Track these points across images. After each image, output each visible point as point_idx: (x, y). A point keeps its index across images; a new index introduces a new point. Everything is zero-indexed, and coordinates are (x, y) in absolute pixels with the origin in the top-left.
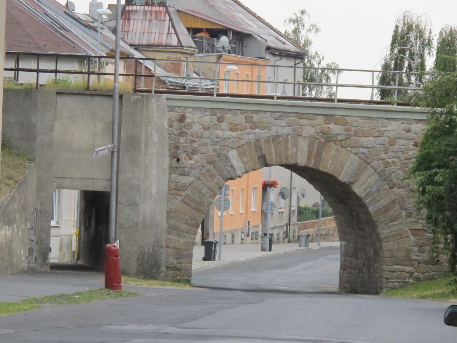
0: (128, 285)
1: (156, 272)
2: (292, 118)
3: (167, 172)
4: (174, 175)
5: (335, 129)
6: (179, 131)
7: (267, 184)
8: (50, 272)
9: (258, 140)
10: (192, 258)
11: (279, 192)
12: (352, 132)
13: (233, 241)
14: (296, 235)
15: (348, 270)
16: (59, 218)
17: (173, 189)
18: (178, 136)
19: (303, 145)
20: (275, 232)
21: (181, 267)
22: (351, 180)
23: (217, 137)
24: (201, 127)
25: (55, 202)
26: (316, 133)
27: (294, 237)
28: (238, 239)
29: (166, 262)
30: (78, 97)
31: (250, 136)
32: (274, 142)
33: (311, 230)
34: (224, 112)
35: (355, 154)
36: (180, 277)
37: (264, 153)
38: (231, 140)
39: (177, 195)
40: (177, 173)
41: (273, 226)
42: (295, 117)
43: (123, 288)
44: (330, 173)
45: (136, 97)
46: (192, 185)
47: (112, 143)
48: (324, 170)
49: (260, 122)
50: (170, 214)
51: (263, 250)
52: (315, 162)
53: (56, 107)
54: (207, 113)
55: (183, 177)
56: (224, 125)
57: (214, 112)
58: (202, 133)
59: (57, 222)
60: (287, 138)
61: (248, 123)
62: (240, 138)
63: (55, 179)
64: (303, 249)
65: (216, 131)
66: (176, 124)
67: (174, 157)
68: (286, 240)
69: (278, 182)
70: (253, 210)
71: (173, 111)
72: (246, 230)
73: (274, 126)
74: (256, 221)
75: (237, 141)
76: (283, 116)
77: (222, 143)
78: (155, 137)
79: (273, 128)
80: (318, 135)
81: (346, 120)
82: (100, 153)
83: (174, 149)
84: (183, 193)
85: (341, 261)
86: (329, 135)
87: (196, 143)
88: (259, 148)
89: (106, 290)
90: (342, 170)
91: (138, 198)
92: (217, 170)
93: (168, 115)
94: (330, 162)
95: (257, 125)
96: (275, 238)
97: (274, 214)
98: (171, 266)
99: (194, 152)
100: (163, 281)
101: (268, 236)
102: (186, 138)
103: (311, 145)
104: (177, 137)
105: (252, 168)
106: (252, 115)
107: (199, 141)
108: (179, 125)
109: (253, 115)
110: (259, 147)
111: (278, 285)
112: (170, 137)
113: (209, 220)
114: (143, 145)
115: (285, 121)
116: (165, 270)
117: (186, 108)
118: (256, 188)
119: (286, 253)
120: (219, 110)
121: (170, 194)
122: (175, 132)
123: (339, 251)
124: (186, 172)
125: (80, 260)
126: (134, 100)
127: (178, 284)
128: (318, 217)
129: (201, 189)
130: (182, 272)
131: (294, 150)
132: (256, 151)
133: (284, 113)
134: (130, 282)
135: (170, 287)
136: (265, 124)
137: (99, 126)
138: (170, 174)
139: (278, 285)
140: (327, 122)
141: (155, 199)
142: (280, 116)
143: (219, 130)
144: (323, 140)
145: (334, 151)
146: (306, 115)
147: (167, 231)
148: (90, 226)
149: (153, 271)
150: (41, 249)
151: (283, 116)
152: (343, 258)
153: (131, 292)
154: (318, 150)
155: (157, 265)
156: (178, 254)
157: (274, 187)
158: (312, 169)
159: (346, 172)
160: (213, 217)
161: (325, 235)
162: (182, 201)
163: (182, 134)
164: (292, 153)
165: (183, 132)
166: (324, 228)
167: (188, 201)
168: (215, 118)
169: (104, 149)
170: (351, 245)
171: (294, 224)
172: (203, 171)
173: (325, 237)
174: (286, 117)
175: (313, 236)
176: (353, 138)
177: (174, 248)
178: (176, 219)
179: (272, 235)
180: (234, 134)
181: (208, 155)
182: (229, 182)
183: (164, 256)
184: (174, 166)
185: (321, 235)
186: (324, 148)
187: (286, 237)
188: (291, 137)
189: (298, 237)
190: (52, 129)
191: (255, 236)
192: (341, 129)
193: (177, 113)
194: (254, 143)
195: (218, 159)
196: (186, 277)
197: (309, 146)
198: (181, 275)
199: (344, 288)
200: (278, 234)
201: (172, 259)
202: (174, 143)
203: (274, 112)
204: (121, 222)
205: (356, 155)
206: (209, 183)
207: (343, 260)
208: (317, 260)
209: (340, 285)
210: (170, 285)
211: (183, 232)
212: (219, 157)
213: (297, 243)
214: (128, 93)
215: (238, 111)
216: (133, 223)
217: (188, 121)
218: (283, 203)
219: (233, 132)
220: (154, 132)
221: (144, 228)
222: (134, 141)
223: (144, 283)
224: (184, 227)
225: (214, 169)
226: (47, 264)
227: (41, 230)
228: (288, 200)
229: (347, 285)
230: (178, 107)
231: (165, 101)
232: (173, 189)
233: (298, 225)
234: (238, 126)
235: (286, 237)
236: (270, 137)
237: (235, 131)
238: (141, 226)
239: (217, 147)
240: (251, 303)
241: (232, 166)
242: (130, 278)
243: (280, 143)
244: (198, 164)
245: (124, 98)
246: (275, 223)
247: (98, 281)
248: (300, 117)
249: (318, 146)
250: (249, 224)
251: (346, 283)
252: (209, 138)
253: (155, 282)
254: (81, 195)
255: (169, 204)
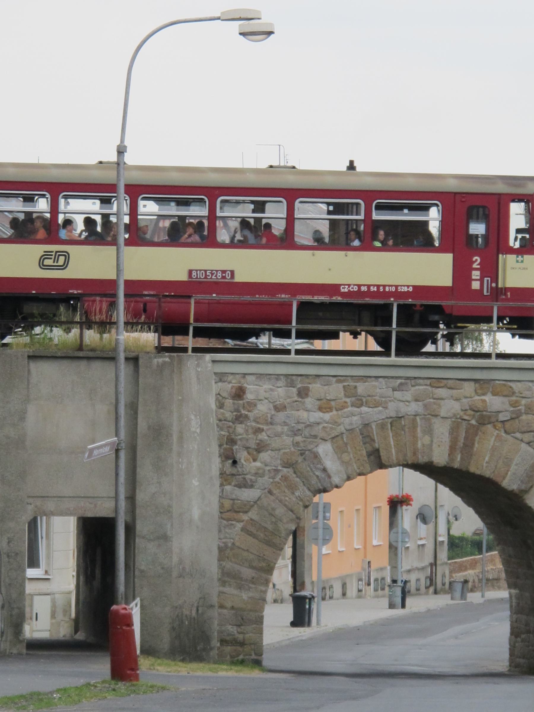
0: (154, 672)
1: (204, 649)
2: (421, 387)
3: (217, 482)
4: (228, 488)
5: (494, 402)
6: (235, 413)
7: (396, 499)
8: (27, 654)
9: (367, 425)
10: (262, 623)
11: (417, 512)
12: (522, 408)
13: (344, 594)
14: (447, 581)
15: (523, 636)
16: (48, 564)
17: (228, 511)
18: (233, 423)
19: (442, 430)
20: (412, 578)
21: (244, 639)
22: (523, 487)
23: (298, 423)
24: (271, 406)
25: (42, 538)
26: (462, 410)
27: (444, 584)
28: (352, 591)
29: (220, 632)
30: (65, 362)
31: (353, 418)
32: (393, 428)
33: (471, 572)
34: (307, 381)
35: (528, 443)
36: (244, 656)
37: (377, 446)
38: (321, 426)
39: (235, 520)
40: (233, 484)
41: (409, 568)
42: (426, 385)
43: (141, 676)
44: (487, 476)
45: (160, 360)
46: (258, 502)
47: (117, 434)
48: (478, 472)
49: (369, 396)
50: (222, 551)
51: (392, 606)
52: (462, 458)
53: (28, 380)
54: (280, 383)
55: (243, 489)
56: (309, 401)
57: (292, 380)
58: (272, 415)
59: (46, 572)
60: (414, 420)
61: (349, 397)
62: (336, 422)
63: (31, 500)
64: (458, 604)
65: (296, 412)
66: (229, 403)
67: (227, 458)
68: (431, 589)
69: (413, 497)
70: (375, 543)
71: (224, 382)
72: (365, 576)
73: (393, 401)
74: (381, 560)
75: (331, 428)
76: (406, 384)
77: (306, 432)
78: (195, 425)
79: (391, 405)
80: (465, 414)
81: (511, 387)
82: (96, 452)
83: (227, 444)
84: (245, 517)
85: (512, 622)
86: (484, 413)
87: (264, 433)
88: (367, 438)
89: (113, 682)
90: (508, 471)
91: (169, 526)
92: (300, 478)
93: (215, 388)
94: (487, 459)
95: (364, 400)
96: (412, 586)
97: (410, 549)
98: (228, 638)
99: (261, 448)
100: (215, 663)
101: (400, 583)
102: (246, 425)
103: (454, 431)
104: (231, 424)
105: (358, 471)
106: (355, 384)
107: (268, 430)
108: (234, 404)
109: (357, 384)
110: (369, 436)
111: (409, 665)
112: (220, 424)
113: (304, 561)
114: (175, 438)
115: (410, 392)
116: (219, 645)
117: (244, 375)
118: (379, 507)
119: (429, 611)
120: (299, 378)
121: (224, 519)
122: (229, 415)
123: (508, 606)
124: (249, 481)
125: (79, 633)
126: (158, 366)
127: (239, 668)
128: (480, 552)
129: (274, 509)
130: (247, 649)
131: (427, 440)
132: (364, 443)
133: (408, 378)
134: (159, 668)
135: (227, 673)
136: (377, 398)
137: (103, 410)
138: (222, 485)
139: (409, 665)
140: (480, 392)
141: (198, 527)
142: (401, 384)
143: (301, 411)
144: (473, 422)
145: (493, 438)
146: (445, 381)
147: (219, 580)
148: (93, 576)
149: (198, 648)
150: (11, 615)
151: (406, 384)
152: (515, 616)
153: (155, 684)
154: (466, 438)
155: (206, 638)
156: (240, 618)
157: (407, 505)
158: (458, 471)
159: (514, 474)
160: (119, 544)
161: (494, 579)
162: (242, 529)
163: (239, 418)
164: (423, 445)
165: (241, 415)
166: (492, 569)
167: (253, 530)
168: (294, 390)
169: (103, 444)
170: (527, 594)
171: (443, 564)
172: (277, 479)
173: (492, 583)
174: (412, 386)
175: (474, 581)
176: (524, 417)
177: (233, 608)
178: (233, 560)
179: (406, 582)
180: (327, 416)
181: (284, 453)
182: (326, 497)
183: (216, 622)
184: (228, 472)
185: (488, 580)
186: (476, 435)
187: (431, 584)
188: (421, 419)
189: (450, 583)
190: (22, 418)
191: (380, 584)
192: (503, 403)
193: (231, 385)
194: (360, 430)
195: (300, 459)
196: (254, 657)
197: (451, 433)
198: (245, 652)
199: (517, 666)
200: (418, 580)
201: (229, 627)
202: (227, 434)
203: (392, 377)
204: (143, 568)
205: (530, 446)
206: (287, 499)
207: (514, 619)
208: (478, 620)
209: (511, 661)
210: (226, 670)
211: (246, 580)
212: (302, 454)
213: (449, 593)
214: (148, 353)
215: (331, 378)
216: (163, 568)
217: (249, 396)
218: (423, 530)
219: (324, 412)
220: (193, 417)
221: (180, 576)
222: (159, 432)
223: (183, 669)
224: (247, 573)
225: (294, 475)
226: (21, 642)
227: (10, 584)
228: (431, 525)
229: (522, 661)
230: (232, 374)
231: (210, 365)
232: (228, 511)
233: (450, 564)
234: (333, 403)
235: (431, 584)
236: (386, 420)
237: (328, 412)
238: (175, 574)
239: (298, 439)
240: (355, 698)
241: (324, 470)
242: (159, 661)
243: (403, 430)
244: (268, 468)
245: (141, 361)
246: (413, 564)
247: (100, 667)
248: (435, 385)
249: (466, 432)
250: (369, 566)
251: (520, 657)
252: (285, 424)
253: (201, 665)
254: (78, 523)
255: (222, 537)
